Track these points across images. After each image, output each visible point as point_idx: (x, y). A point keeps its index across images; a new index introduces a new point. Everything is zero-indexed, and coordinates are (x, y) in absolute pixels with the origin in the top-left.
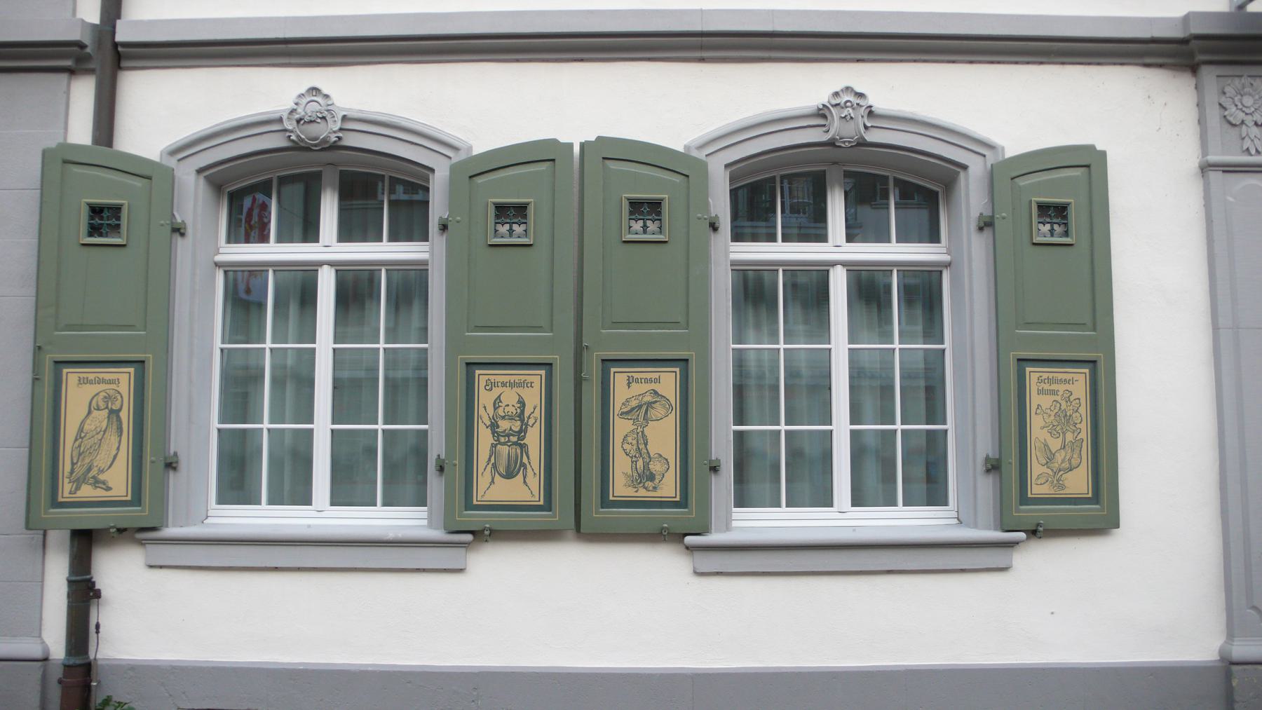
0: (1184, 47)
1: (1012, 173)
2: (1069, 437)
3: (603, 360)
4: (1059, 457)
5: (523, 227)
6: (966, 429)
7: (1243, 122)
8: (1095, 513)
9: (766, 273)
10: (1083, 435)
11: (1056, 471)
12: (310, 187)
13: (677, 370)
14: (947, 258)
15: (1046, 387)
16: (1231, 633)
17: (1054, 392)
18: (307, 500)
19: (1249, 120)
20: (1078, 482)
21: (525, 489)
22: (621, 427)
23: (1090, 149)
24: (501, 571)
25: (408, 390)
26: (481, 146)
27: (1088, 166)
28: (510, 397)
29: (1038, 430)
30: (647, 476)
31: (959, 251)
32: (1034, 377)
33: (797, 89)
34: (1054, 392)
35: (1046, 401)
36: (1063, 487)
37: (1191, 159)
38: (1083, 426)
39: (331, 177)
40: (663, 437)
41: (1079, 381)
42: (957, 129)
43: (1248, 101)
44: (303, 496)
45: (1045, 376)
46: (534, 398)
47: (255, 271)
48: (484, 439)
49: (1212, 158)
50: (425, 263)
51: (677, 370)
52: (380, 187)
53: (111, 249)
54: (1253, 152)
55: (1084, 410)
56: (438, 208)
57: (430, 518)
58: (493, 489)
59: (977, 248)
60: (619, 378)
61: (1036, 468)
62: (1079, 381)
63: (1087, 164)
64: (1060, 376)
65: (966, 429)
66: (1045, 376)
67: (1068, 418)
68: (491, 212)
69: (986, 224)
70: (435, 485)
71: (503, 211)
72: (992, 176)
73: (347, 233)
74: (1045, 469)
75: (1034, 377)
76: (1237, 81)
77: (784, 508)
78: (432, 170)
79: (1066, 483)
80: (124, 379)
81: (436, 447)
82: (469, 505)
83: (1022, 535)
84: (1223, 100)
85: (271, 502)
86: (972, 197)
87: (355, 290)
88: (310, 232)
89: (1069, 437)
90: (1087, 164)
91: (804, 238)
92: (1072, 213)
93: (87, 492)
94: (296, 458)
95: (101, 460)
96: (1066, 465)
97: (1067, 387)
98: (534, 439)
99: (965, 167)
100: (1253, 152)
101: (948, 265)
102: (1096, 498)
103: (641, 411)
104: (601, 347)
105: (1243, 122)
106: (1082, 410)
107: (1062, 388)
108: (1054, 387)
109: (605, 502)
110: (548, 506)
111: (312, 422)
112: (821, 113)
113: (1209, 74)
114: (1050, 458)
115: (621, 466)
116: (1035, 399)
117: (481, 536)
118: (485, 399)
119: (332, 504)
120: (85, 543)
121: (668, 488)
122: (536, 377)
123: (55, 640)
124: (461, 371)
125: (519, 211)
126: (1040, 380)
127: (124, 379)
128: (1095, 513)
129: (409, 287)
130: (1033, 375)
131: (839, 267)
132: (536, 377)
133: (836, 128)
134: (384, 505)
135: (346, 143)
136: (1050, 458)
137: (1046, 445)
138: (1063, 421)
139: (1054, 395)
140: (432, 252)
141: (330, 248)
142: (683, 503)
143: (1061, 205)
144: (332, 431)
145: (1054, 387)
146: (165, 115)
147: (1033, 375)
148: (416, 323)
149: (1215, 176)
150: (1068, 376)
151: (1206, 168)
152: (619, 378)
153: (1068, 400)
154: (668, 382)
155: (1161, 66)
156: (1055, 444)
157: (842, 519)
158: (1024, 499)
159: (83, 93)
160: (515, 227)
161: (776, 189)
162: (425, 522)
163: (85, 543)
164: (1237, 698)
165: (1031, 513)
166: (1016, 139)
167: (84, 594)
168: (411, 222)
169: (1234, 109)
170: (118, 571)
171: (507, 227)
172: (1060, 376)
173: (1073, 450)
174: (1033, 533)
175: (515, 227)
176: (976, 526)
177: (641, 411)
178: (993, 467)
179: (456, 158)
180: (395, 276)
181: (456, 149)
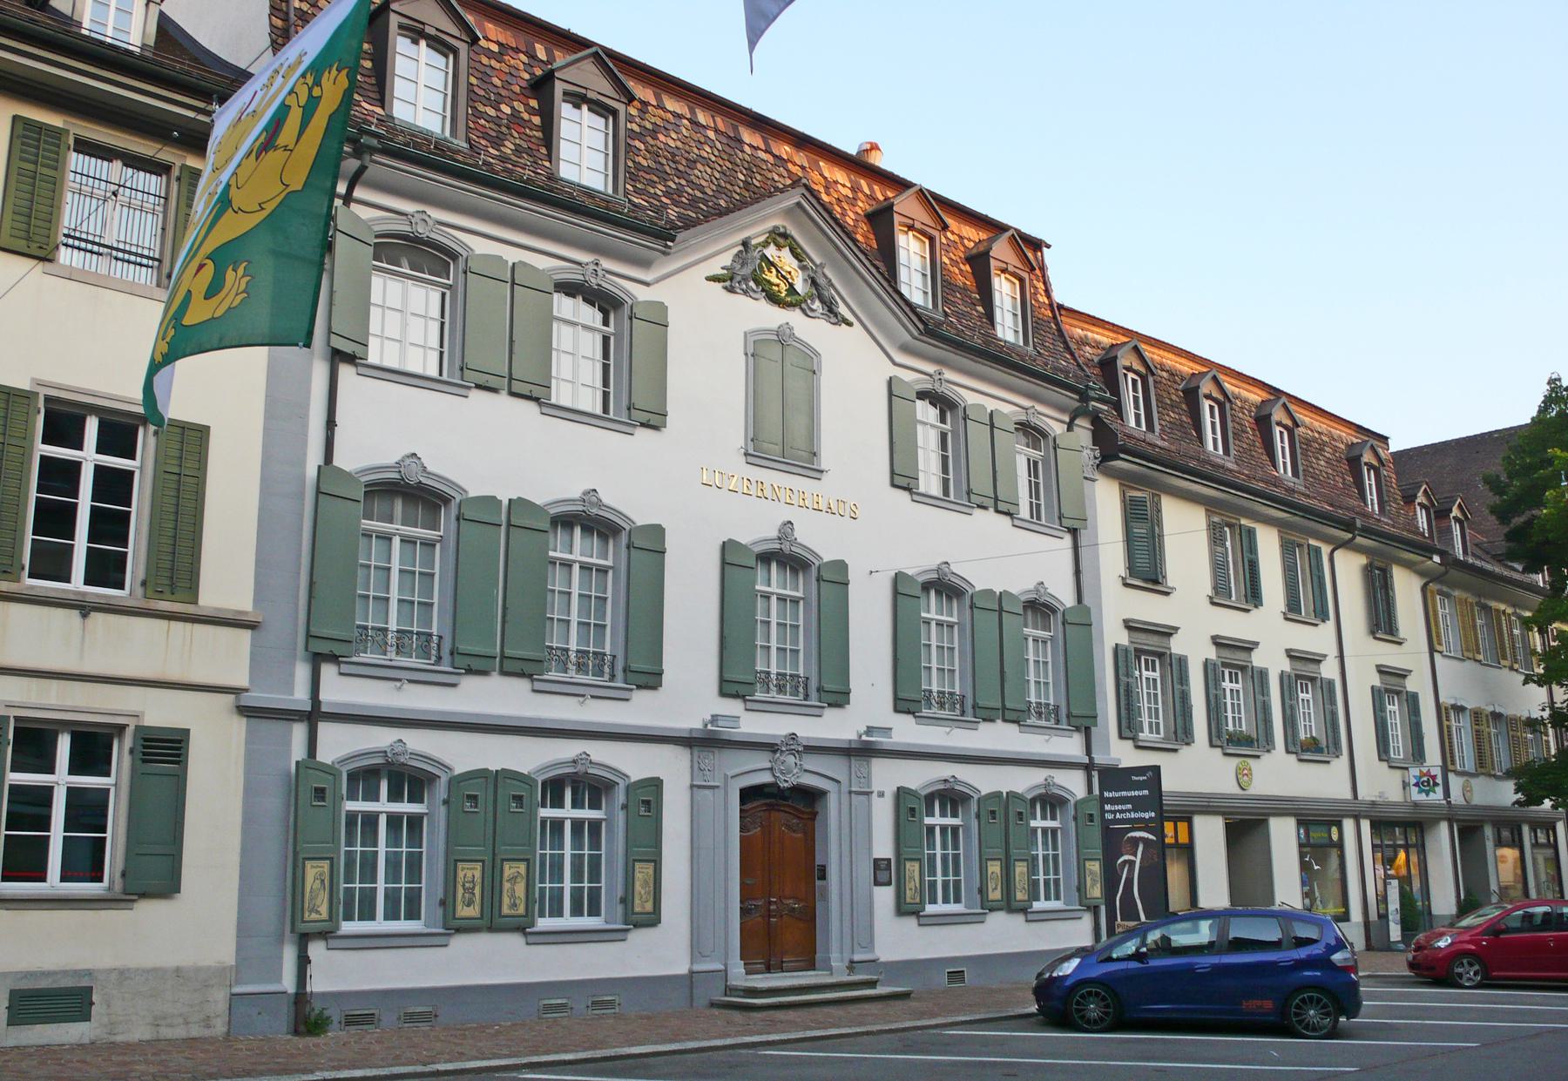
6: (430, 886)
8: (652, 919)
11: (642, 904)
20: (649, 907)
21: (473, 911)
22: (507, 886)
24: (462, 944)
28: (469, 874)
30: (514, 905)
31: (611, 814)
33: (567, 750)
37: (688, 782)
40: (520, 889)
44: (561, 915)
46: (478, 874)
48: (460, 891)
52: (409, 779)
58: (464, 911)
59: (620, 817)
60: (506, 866)
61: (637, 901)
65: (430, 886)
69: (446, 802)
72: (628, 788)
73: (575, 805)
80: (326, 864)
93: (314, 916)
94: (557, 897)
95: (318, 902)
98: (477, 891)
103: (513, 880)
104: (503, 849)
110: (482, 917)
112: (574, 762)
113: (696, 750)
115: (506, 900)
116: (638, 875)
117: (459, 930)
118: (461, 874)
120: (304, 940)
121: (521, 910)
122: (479, 866)
123: (288, 983)
127: (326, 864)
132: (479, 866)
133: (580, 768)
138: (646, 882)
139: (643, 872)
141: (383, 806)
143: (649, 794)
146: (337, 744)
151: (692, 786)
152: (506, 866)
154: (522, 867)
157: (380, 925)
159: (299, 732)
161: (554, 789)
163: (304, 940)
165: (457, 923)
166: (636, 775)
167: (303, 961)
170: (316, 950)
177: (513, 880)
178: (443, 903)
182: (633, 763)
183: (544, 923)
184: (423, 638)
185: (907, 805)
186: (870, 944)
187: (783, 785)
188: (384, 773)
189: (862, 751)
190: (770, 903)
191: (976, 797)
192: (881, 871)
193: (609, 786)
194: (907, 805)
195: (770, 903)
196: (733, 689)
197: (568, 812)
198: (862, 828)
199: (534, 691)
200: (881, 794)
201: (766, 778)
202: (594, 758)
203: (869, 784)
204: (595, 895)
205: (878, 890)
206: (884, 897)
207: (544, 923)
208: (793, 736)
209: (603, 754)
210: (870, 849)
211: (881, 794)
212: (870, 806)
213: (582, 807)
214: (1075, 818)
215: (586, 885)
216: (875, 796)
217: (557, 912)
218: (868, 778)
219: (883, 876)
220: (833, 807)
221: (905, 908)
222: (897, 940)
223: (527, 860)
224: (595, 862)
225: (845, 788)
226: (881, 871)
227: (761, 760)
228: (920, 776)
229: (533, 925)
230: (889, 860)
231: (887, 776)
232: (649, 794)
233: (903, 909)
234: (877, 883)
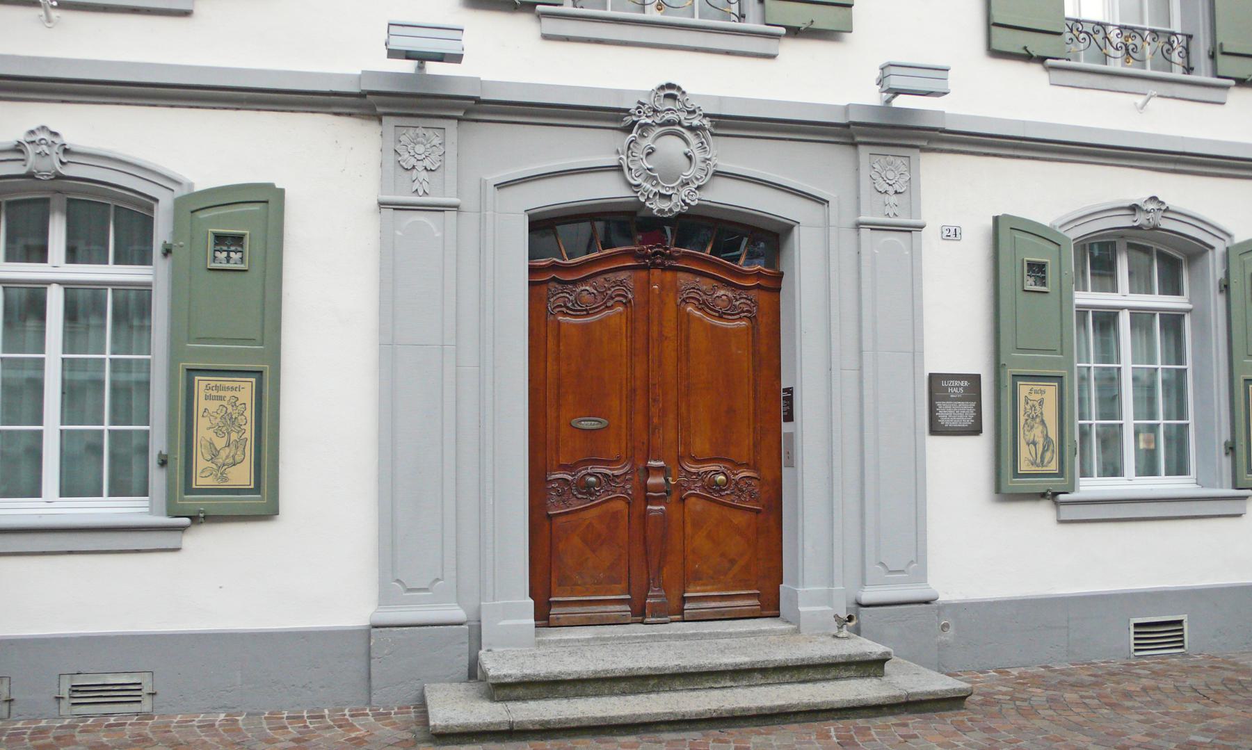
0: (845, 130)
1: (196, 205)
2: (234, 436)
3: (188, 370)
4: (223, 454)
5: (239, 255)
7: (414, 167)
8: (258, 502)
9: (80, 292)
10: (247, 435)
12: (41, 210)
13: (254, 380)
14: (1190, 306)
15: (214, 393)
16: (385, 598)
17: (221, 398)
18: (36, 492)
19: (419, 166)
20: (242, 475)
23: (270, 187)
25: (131, 397)
26: (201, 184)
27: (266, 202)
29: (204, 430)
32: (203, 385)
34: (221, 398)
35: (213, 406)
36: (226, 479)
38: (248, 427)
39: (57, 202)
41: (245, 389)
42: (110, 155)
43: (420, 149)
45: (213, 384)
47: (97, 289)
49: (863, 218)
50: (149, 284)
51: (254, 380)
53: (222, 273)
54: (421, 193)
55: (249, 414)
56: (162, 232)
57: (151, 507)
61: (201, 463)
62: (245, 389)
63: (266, 201)
64: (227, 384)
66: (213, 384)
67: (233, 421)
68: (211, 240)
70: (157, 478)
71: (220, 239)
72: (179, 203)
74: (210, 464)
75: (203, 385)
76: (411, 131)
77: (1096, 478)
78: (157, 200)
79: (229, 476)
81: (158, 445)
82: (189, 489)
83: (186, 521)
84: (398, 147)
85: (112, 494)
86: (1214, 268)
87: (82, 304)
88: (39, 253)
89: (234, 436)
90: (266, 201)
91: (1103, 289)
92: (1049, 269)
94: (1111, 439)
96: (230, 460)
97: (234, 393)
99: (1212, 248)
100: (421, 193)
101: (1189, 311)
102: (257, 489)
105: (414, 167)
106: (247, 413)
107: (228, 394)
108: (221, 393)
109: (1016, 475)
111: (41, 424)
112: (18, 148)
114: (215, 454)
116: (201, 403)
119: (61, 496)
124: (182, 376)
125: (238, 240)
126: (208, 388)
128: (258, 502)
129: (133, 308)
130: (201, 383)
131: (54, 286)
134: (110, 495)
135: (1163, 226)
136: (215, 454)
137: (211, 443)
138: (229, 422)
140: (155, 275)
142: (1061, 474)
143: (242, 230)
144: (61, 431)
145: (221, 393)
147: (201, 383)
148: (30, 336)
149: (865, 232)
150: (235, 385)
151: (382, 204)
153: (234, 405)
155: (350, 115)
156: (220, 443)
158: (189, 489)
160: (232, 254)
161: (1099, 256)
162: (147, 510)
164: (373, 655)
168: (135, 248)
169: (407, 155)
171: (225, 254)
172: (227, 384)
173: (237, 448)
174: (195, 519)
175: (232, 254)
176: (1221, 487)
179: (179, 192)
180: (121, 294)
181: (178, 183)
182: (192, 154)
183: (1092, 486)
184: (1163, 40)
185: (1021, 263)
186: (917, 564)
187: (657, 206)
188: (57, 202)
189: (890, 134)
190: (648, 471)
191: (1220, 247)
192: (950, 403)
193: (1196, 251)
194: (1021, 263)
195: (648, 471)
196: (1014, 42)
197: (1123, 297)
198: (895, 302)
199: (546, 37)
200: (953, 234)
201: (608, 190)
202: (1171, 202)
203: (914, 208)
204: (1178, 439)
205: (939, 446)
206: (961, 463)
207: (1092, 486)
208: (670, 91)
209: (1190, 197)
210: (916, 354)
211: (953, 234)
212: (915, 257)
213: (1149, 291)
214: (1225, 287)
215: (106, 427)
216: (930, 239)
217: (1113, 469)
218: (908, 192)
219: (951, 413)
220: (808, 265)
221: (1011, 484)
222: (982, 549)
223: (1059, 378)
224: (1176, 385)
225: (841, 213)
226: (950, 403)
227: (599, 147)
228: (1061, 199)
229: (1071, 488)
230: (975, 379)
231: (960, 200)
232: (242, 230)
233: (1009, 486)
234: (936, 429)
